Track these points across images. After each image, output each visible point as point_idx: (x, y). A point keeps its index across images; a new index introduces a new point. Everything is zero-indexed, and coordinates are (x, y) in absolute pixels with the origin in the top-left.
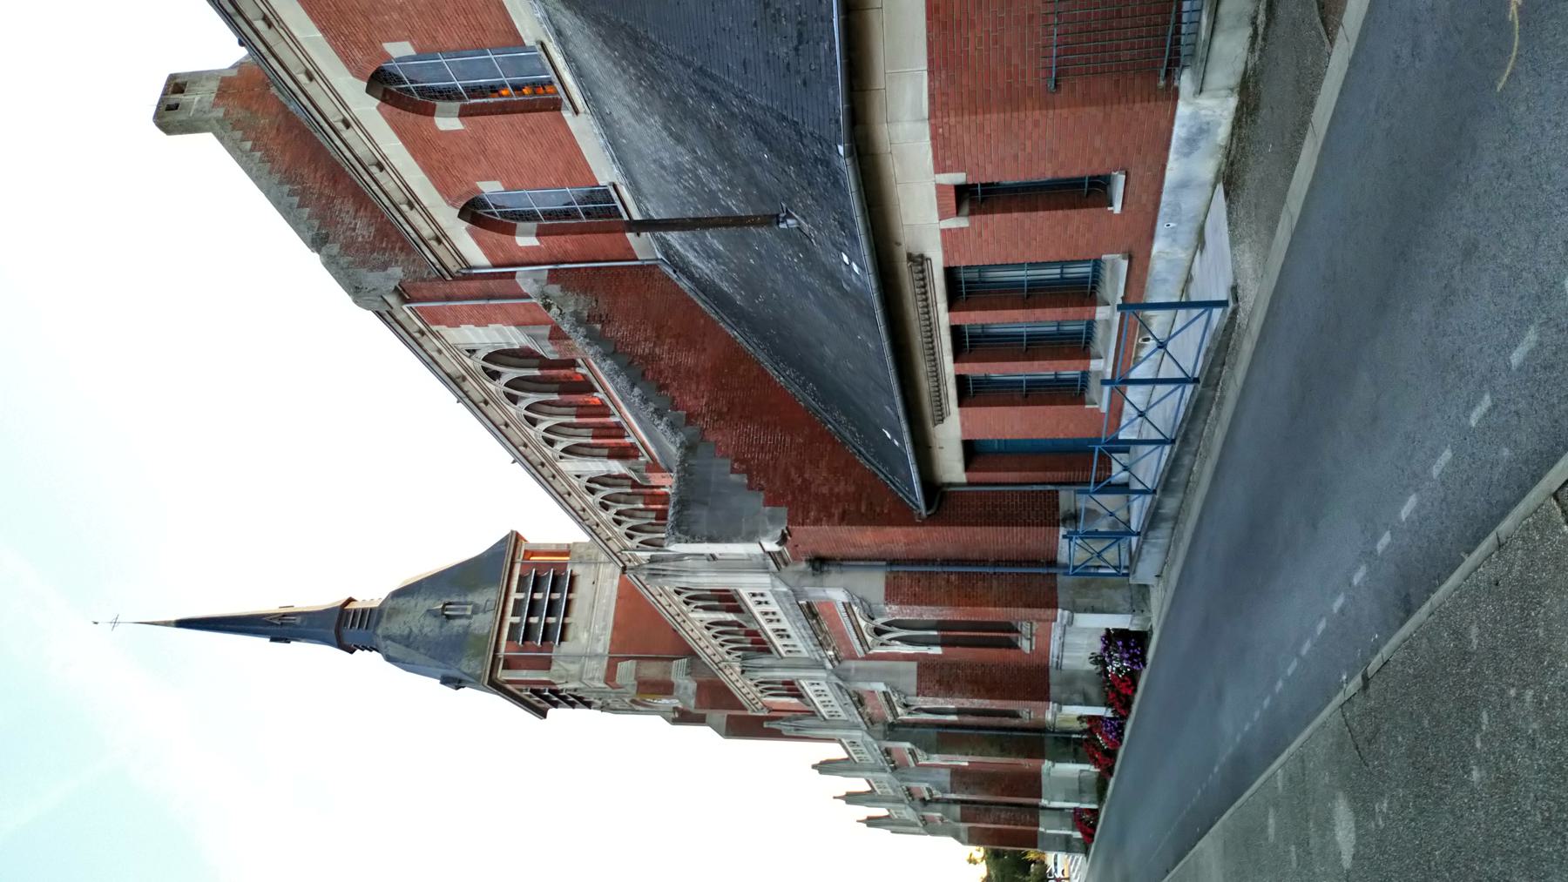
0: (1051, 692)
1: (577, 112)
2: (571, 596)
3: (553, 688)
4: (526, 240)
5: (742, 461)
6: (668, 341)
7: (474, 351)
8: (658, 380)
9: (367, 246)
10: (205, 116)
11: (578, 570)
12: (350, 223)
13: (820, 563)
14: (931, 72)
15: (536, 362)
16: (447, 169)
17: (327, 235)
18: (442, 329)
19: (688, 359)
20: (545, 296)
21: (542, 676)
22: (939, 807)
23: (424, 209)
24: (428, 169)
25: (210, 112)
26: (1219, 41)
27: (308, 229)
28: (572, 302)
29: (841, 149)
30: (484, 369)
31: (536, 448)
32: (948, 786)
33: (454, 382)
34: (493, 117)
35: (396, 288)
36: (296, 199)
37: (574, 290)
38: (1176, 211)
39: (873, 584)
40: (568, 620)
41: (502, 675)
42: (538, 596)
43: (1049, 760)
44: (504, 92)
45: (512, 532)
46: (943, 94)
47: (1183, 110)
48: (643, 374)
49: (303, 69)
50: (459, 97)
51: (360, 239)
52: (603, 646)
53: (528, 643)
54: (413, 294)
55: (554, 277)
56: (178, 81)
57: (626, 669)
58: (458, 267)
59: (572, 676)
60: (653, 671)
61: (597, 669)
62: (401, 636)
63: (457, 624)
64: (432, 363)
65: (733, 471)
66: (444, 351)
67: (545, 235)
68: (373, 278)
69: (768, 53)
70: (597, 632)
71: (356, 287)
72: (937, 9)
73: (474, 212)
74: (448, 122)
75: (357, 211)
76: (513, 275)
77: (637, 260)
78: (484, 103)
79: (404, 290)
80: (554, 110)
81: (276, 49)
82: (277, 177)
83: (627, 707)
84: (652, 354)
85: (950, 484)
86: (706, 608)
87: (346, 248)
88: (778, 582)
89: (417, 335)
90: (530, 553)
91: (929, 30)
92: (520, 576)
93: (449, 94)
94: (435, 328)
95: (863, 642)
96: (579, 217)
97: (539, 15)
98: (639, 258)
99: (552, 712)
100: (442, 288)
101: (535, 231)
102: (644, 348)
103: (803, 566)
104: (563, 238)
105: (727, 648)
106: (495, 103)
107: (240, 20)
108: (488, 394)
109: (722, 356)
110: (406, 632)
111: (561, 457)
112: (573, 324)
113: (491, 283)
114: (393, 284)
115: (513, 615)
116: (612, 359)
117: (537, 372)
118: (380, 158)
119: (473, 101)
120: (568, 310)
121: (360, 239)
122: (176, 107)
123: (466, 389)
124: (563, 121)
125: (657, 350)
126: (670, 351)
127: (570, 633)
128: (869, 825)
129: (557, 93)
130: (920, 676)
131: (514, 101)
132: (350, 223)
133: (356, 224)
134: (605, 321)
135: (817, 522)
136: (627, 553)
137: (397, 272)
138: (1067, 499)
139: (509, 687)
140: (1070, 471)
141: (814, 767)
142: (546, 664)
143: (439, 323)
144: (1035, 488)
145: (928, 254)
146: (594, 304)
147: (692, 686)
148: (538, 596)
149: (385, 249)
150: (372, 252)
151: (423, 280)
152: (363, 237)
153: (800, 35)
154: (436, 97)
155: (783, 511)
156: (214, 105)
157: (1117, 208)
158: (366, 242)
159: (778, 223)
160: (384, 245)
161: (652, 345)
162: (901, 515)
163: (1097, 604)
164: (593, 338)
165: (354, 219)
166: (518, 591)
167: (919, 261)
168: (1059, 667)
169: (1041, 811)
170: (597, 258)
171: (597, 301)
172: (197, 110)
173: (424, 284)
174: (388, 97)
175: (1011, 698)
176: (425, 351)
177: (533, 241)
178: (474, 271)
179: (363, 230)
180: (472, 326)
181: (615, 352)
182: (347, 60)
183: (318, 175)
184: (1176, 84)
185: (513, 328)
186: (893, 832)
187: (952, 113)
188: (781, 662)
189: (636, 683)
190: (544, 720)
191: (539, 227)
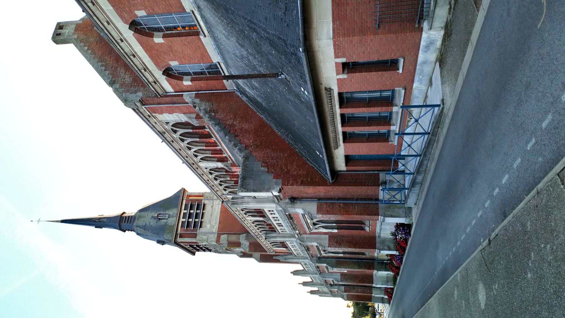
0: (377, 246)
1: (205, 36)
2: (204, 211)
3: (197, 244)
4: (187, 83)
5: (265, 163)
7: (168, 123)
8: (235, 133)
11: (206, 202)
12: (123, 77)
13: (293, 200)
14: (333, 21)
15: (191, 127)
17: (115, 81)
19: (245, 126)
21: (193, 240)
22: (336, 287)
23: (150, 71)
24: (151, 57)
25: (72, 36)
27: (108, 78)
28: (204, 105)
30: (172, 129)
31: (191, 158)
32: (340, 280)
33: (161, 134)
34: (175, 38)
35: (140, 100)
36: (104, 68)
38: (422, 70)
39: (313, 207)
40: (202, 220)
41: (179, 240)
42: (192, 211)
43: (376, 270)
44: (179, 29)
45: (182, 188)
46: (337, 30)
47: (424, 35)
48: (230, 131)
50: (162, 31)
51: (127, 82)
52: (215, 229)
53: (188, 228)
55: (197, 96)
56: (61, 25)
57: (224, 238)
58: (162, 93)
59: (204, 240)
60: (233, 238)
61: (213, 238)
64: (153, 127)
65: (262, 166)
66: (157, 122)
67: (194, 81)
68: (131, 97)
69: (274, 15)
70: (213, 224)
73: (168, 72)
74: (158, 40)
75: (125, 72)
77: (227, 90)
78: (171, 33)
80: (197, 35)
85: (340, 171)
86: (252, 216)
87: (122, 85)
88: (278, 207)
89: (147, 117)
91: (333, 6)
92: (185, 204)
93: (159, 30)
94: (154, 114)
95: (309, 228)
100: (156, 100)
101: (190, 79)
102: (230, 122)
103: (287, 200)
105: (260, 230)
110: (144, 224)
111: (200, 161)
112: (204, 113)
113: (174, 98)
114: (138, 99)
117: (191, 131)
119: (167, 32)
121: (127, 82)
123: (165, 137)
124: (200, 39)
127: (204, 225)
128: (311, 294)
133: (125, 77)
134: (216, 112)
136: (224, 196)
137: (140, 94)
139: (182, 244)
141: (291, 273)
142: (195, 236)
143: (155, 113)
144: (371, 172)
145: (332, 88)
146: (212, 106)
147: (247, 244)
148: (192, 211)
149: (136, 86)
150: (131, 87)
151: (150, 97)
152: (128, 81)
153: (286, 8)
155: (280, 181)
156: (74, 34)
158: (129, 84)
159: (278, 77)
160: (135, 84)
162: (323, 182)
163: (393, 214)
164: (211, 118)
166: (185, 210)
167: (329, 90)
168: (379, 237)
169: (373, 289)
171: (213, 105)
172: (67, 36)
174: (137, 31)
175: (362, 248)
176: (150, 123)
178: (168, 94)
180: (167, 114)
181: (219, 123)
182: (122, 17)
183: (111, 59)
184: (422, 26)
185: (182, 114)
187: (341, 36)
188: (280, 235)
189: (227, 242)
190: (194, 256)
191: (192, 78)
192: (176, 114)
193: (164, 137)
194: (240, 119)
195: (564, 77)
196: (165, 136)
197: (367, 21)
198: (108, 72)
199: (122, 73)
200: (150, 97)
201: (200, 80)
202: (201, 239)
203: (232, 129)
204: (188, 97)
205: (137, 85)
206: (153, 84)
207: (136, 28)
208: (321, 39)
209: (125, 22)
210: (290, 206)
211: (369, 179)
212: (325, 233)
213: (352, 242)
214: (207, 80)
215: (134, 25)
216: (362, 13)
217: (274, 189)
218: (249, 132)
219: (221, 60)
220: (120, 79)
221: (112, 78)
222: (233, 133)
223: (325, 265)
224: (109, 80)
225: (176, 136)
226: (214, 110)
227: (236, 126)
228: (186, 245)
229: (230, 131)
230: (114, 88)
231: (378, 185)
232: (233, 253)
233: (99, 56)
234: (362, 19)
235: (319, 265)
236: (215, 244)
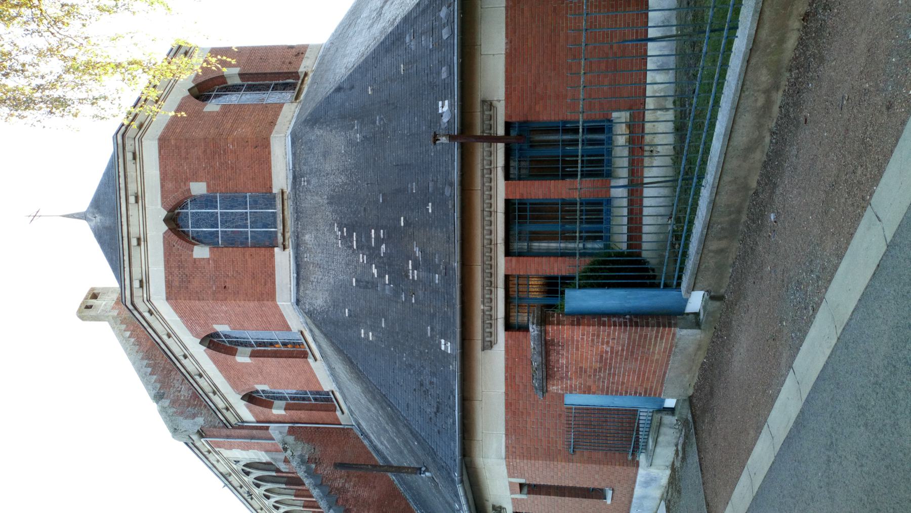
1: (316, 360)
4: (278, 411)
6: (353, 479)
7: (239, 461)
8: (345, 506)
9: (186, 403)
10: (106, 314)
12: (178, 387)
14: (507, 435)
16: (238, 378)
17: (164, 394)
18: (222, 450)
19: (364, 493)
23: (222, 395)
24: (228, 378)
25: (110, 312)
26: (658, 450)
27: (153, 389)
28: (300, 449)
29: (456, 475)
30: (243, 470)
31: (268, 510)
33: (225, 477)
34: (269, 359)
35: (198, 431)
36: (149, 370)
37: (302, 441)
44: (277, 346)
46: (513, 447)
47: (641, 472)
48: (337, 501)
49: (166, 332)
50: (251, 346)
51: (182, 398)
54: (208, 433)
55: (291, 431)
56: (95, 292)
58: (236, 421)
64: (213, 467)
66: (221, 460)
67: (290, 409)
69: (420, 407)
71: (175, 429)
72: (511, 404)
73: (251, 398)
74: (243, 358)
76: (267, 428)
77: (341, 424)
78: (265, 350)
79: (202, 431)
80: (304, 357)
81: (153, 325)
82: (141, 355)
87: (173, 403)
89: (206, 453)
91: (506, 414)
93: (246, 344)
94: (217, 449)
96: (310, 400)
97: (302, 320)
98: (342, 423)
100: (225, 432)
101: (284, 407)
102: (339, 483)
104: (300, 412)
106: (271, 350)
107: (136, 313)
108: (243, 482)
109: (385, 493)
112: (298, 463)
113: (254, 432)
114: (198, 428)
116: (320, 489)
118: (201, 372)
119: (259, 348)
120: (297, 454)
121: (182, 398)
122: (91, 307)
123: (230, 480)
124: (308, 364)
125: (347, 485)
126: (354, 486)
129: (305, 348)
131: (282, 351)
132: (178, 387)
133: (181, 388)
134: (318, 462)
137: (200, 420)
140: (644, 56)
143: (220, 447)
145: (504, 506)
146: (312, 451)
149: (195, 406)
150: (188, 407)
151: (215, 427)
152: (185, 396)
153: (438, 408)
154: (239, 345)
156: (113, 308)
157: (609, 501)
158: (186, 400)
159: (420, 474)
160: (195, 403)
161: (344, 481)
165: (181, 385)
170: (318, 422)
171: (314, 449)
172: (103, 310)
173: (215, 429)
174: (211, 345)
176: (209, 461)
177: (283, 412)
178: (245, 424)
180: (239, 450)
181: (321, 484)
182: (192, 330)
184: (637, 459)
185: (263, 452)
187: (518, 457)
191: (287, 405)
192: (254, 451)
193: (227, 480)
194: (356, 479)
195: (910, 374)
196: (231, 479)
197: (556, 441)
198: (155, 377)
199: (178, 380)
200: (215, 427)
201: (300, 410)
203: (341, 496)
205: (199, 403)
206: (224, 411)
207: (211, 341)
208: (488, 458)
209: (197, 336)
214: (311, 410)
215: (212, 342)
216: (548, 429)
218: (369, 505)
219: (336, 388)
220: (172, 390)
221: (160, 389)
222: (342, 505)
224: (154, 392)
225: (249, 479)
226: (316, 459)
227: (348, 491)
229: (337, 501)
230: (159, 406)
231: (617, 391)
234: (549, 437)
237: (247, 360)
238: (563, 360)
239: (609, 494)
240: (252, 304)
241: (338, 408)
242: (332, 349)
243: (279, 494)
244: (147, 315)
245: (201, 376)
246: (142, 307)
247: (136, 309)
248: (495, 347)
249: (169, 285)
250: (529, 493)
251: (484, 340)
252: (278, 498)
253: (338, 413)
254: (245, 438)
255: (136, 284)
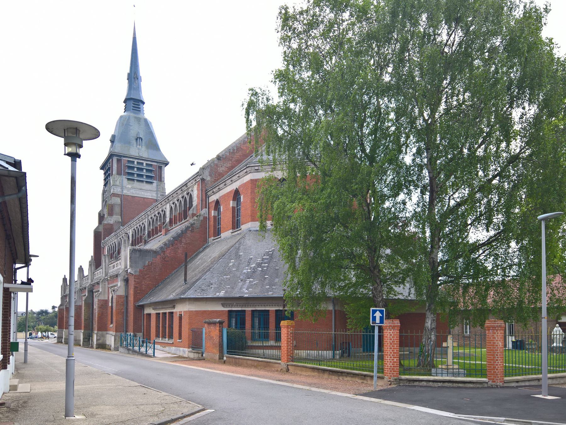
2: (145, 182)
3: (111, 175)
4: (213, 213)
5: (151, 264)
11: (155, 185)
13: (126, 281)
20: (200, 215)
21: (115, 172)
33: (186, 184)
38: (177, 350)
39: (121, 292)
47: (187, 349)
52: (125, 192)
55: (205, 218)
57: (118, 200)
59: (115, 182)
60: (117, 209)
61: (118, 190)
62: (130, 122)
63: (134, 142)
64: (189, 180)
65: (149, 262)
68: (207, 172)
73: (217, 203)
74: (232, 204)
75: (227, 167)
76: (206, 208)
83: (105, 199)
84: (182, 242)
85: (144, 310)
86: (133, 235)
88: (122, 270)
90: (160, 168)
95: (112, 287)
99: (102, 172)
102: (184, 240)
103: (126, 276)
114: (205, 178)
115: (137, 162)
130: (104, 300)
135: (135, 281)
137: (208, 178)
138: (140, 335)
141: (81, 266)
142: (119, 173)
147: (112, 222)
148: (145, 171)
155: (138, 273)
157: (178, 341)
162: (136, 300)
163: (117, 341)
164: (187, 228)
166: (146, 164)
167: (174, 307)
168: (107, 334)
175: (98, 322)
177: (213, 215)
179: (221, 170)
186: (62, 286)
188: (107, 265)
191: (235, 207)
202: (116, 179)
204: (204, 211)
210: (122, 278)
211: (491, 377)
212: (108, 297)
213: (102, 316)
215: (236, 194)
217: (132, 270)
223: (87, 295)
228: (110, 163)
232: (103, 206)
233: (241, 147)
235: (87, 289)
236: (112, 192)
237: (231, 206)
238: (212, 327)
239: (180, 341)
240: (250, 212)
241: (216, 238)
242: (188, 303)
243: (179, 206)
244: (245, 171)
245: (225, 185)
246: (248, 170)
247: (247, 168)
248: (223, 307)
249: (256, 180)
250: (179, 317)
251: (225, 304)
252: (178, 205)
253: (213, 238)
254: (202, 198)
255: (256, 168)
